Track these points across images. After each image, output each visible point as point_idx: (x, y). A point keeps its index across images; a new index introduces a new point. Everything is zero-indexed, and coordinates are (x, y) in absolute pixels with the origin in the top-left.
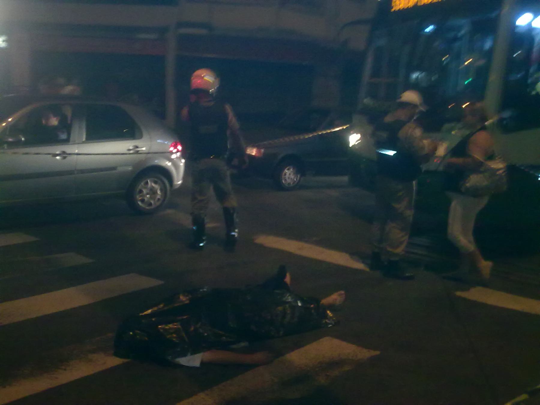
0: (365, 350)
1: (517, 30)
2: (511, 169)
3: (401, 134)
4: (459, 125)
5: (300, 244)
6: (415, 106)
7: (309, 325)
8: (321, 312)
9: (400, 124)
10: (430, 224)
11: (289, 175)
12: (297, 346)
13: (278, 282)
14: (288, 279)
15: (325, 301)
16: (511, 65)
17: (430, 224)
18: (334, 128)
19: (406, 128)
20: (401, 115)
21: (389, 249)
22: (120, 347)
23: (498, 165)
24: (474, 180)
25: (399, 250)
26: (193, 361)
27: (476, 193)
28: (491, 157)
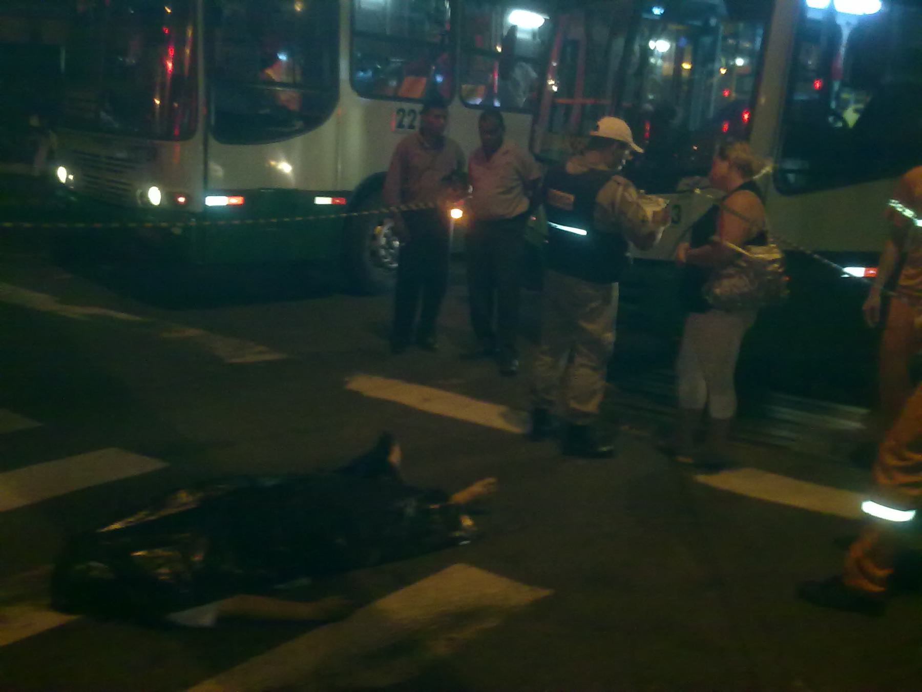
0: (526, 588)
1: (810, 15)
2: (792, 258)
3: (603, 197)
4: (705, 181)
5: (427, 391)
6: (623, 145)
7: (428, 544)
8: (451, 516)
9: (597, 180)
10: (644, 365)
11: (698, 191)
12: (401, 581)
13: (373, 465)
14: (395, 457)
15: (461, 497)
16: (795, 74)
17: (644, 365)
18: (230, 207)
19: (610, 186)
20: (595, 161)
21: (574, 405)
22: (63, 593)
23: (768, 254)
24: (727, 286)
25: (592, 407)
26: (205, 616)
27: (728, 306)
28: (760, 239)
